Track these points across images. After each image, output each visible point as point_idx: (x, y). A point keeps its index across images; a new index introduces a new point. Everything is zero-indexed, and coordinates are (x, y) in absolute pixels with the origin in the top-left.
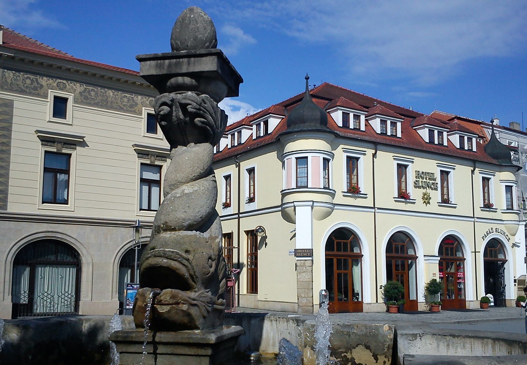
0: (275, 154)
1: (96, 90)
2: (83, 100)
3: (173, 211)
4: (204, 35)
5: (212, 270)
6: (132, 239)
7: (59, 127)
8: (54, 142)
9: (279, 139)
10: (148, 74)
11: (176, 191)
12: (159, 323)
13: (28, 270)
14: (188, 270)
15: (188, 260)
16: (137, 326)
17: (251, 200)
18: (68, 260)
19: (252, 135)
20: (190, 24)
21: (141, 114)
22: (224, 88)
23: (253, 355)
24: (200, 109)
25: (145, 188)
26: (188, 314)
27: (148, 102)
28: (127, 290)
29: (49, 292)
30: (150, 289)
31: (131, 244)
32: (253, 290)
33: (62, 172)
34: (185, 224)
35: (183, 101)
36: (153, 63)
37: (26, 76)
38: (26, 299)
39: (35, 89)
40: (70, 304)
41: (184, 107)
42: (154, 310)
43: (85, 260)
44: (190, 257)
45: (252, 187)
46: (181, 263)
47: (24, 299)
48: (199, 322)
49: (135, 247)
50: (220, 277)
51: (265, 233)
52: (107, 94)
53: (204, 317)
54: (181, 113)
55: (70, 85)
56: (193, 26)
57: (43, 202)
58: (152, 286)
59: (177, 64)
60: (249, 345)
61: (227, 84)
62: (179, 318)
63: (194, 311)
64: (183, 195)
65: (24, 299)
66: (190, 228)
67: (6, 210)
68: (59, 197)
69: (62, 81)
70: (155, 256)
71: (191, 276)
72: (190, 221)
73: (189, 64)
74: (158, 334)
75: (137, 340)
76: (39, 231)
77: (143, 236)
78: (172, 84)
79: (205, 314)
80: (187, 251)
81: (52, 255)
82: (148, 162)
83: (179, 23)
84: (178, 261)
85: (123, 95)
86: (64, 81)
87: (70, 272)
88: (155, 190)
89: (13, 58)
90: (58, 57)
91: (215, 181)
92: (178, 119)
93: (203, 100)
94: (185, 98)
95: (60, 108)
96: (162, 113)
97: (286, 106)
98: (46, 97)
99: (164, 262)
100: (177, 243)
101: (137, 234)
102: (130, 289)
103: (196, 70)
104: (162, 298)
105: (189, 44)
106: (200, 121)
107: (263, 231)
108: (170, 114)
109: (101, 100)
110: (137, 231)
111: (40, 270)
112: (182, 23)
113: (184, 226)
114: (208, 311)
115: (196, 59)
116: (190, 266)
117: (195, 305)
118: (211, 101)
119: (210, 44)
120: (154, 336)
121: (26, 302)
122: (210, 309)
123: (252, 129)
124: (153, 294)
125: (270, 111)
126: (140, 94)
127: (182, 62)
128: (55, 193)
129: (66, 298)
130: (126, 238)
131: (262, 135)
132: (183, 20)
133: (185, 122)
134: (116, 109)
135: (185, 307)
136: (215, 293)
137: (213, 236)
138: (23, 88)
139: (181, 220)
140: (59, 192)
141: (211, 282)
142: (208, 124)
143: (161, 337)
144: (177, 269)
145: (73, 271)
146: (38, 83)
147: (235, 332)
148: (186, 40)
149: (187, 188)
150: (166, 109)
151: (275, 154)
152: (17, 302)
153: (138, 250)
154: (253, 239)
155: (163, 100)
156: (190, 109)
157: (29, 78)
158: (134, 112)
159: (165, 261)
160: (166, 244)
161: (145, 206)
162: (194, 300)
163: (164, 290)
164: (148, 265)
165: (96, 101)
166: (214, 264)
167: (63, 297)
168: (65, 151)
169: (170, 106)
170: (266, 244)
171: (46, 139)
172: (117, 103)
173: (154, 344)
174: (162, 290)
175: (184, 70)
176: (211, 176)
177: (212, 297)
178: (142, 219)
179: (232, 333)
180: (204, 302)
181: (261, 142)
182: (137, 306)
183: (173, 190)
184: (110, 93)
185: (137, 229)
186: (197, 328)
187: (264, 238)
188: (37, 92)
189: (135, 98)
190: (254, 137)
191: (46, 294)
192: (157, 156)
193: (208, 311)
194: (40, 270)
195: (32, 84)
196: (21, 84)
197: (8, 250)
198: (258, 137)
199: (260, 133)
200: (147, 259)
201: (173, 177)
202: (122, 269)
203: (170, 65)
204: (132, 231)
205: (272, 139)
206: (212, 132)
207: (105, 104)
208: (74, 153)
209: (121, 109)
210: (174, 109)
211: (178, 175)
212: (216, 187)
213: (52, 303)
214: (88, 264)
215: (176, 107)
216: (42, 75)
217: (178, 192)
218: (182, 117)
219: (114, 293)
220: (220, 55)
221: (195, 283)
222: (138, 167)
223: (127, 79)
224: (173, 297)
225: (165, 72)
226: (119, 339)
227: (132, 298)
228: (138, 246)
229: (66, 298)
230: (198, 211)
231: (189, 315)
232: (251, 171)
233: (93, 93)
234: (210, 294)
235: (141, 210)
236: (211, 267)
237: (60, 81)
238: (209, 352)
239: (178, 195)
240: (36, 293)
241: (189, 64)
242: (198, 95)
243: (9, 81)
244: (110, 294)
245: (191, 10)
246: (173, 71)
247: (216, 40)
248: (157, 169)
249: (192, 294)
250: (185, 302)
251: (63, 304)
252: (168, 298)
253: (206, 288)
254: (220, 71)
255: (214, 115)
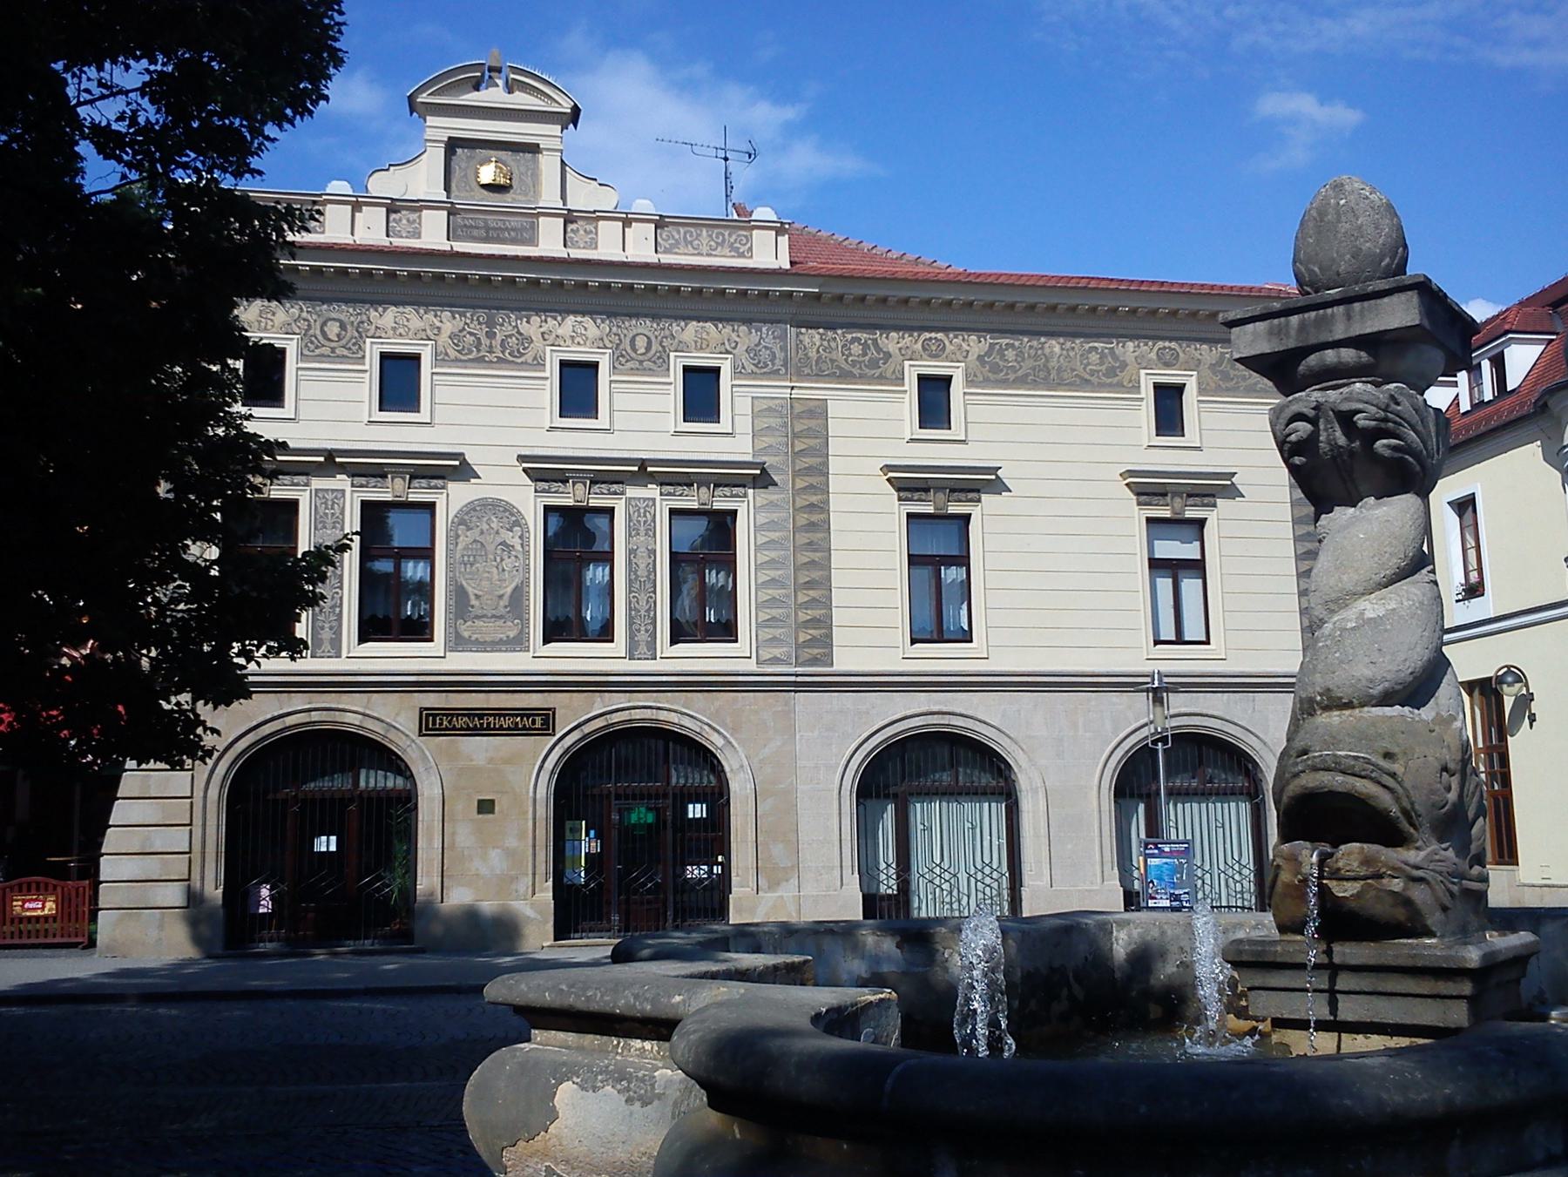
0: (1533, 451)
1: (1017, 344)
2: (991, 375)
3: (1342, 662)
4: (1374, 242)
5: (1452, 796)
6: (1146, 720)
7: (937, 453)
8: (927, 490)
9: (1545, 405)
10: (1253, 353)
11: (1343, 614)
12: (1340, 922)
13: (890, 808)
14: (1397, 799)
15: (1393, 775)
16: (1282, 929)
17: (1473, 590)
18: (984, 782)
19: (1456, 401)
20: (1339, 221)
21: (1136, 388)
22: (1438, 357)
23: (1554, 1014)
24: (1386, 420)
25: (1164, 585)
26: (1406, 902)
27: (1153, 355)
28: (1147, 856)
29: (946, 865)
30: (1308, 844)
31: (1145, 732)
32: (1501, 856)
33: (951, 561)
34: (1374, 692)
35: (1345, 407)
36: (1261, 326)
37: (849, 337)
38: (892, 882)
39: (874, 364)
40: (999, 894)
41: (1346, 419)
42: (1324, 892)
43: (1026, 780)
44: (1397, 767)
45: (1472, 554)
46: (1379, 783)
47: (888, 885)
48: (1434, 919)
49: (1155, 742)
50: (1471, 814)
51: (1527, 686)
52: (1047, 351)
53: (1445, 909)
54: (1339, 433)
55: (952, 342)
56: (1348, 226)
57: (913, 642)
58: (1312, 838)
59: (1318, 323)
60: (1541, 992)
61: (1441, 346)
62: (1383, 910)
63: (1418, 894)
64: (1364, 622)
65: (888, 885)
66: (1386, 699)
67: (832, 665)
68: (949, 625)
69: (933, 335)
70: (1315, 769)
71: (1405, 812)
72: (1387, 684)
73: (1349, 317)
74: (1337, 948)
75: (1288, 960)
76: (909, 713)
77: (1172, 712)
78: (1310, 369)
79: (1447, 901)
80: (1388, 755)
81: (944, 770)
82: (1165, 513)
83: (1311, 224)
84: (1371, 779)
85: (1087, 346)
86: (940, 335)
87: (992, 813)
88: (1190, 586)
89: (818, 297)
90: (920, 276)
91: (1436, 583)
92: (1334, 446)
93: (1392, 397)
94: (1347, 399)
95: (934, 401)
96: (1293, 438)
97: (1555, 305)
98: (900, 380)
99: (1338, 782)
100: (1362, 737)
101: (1158, 709)
102: (1153, 856)
103: (1368, 331)
104: (1340, 864)
105: (1342, 269)
106: (1388, 446)
107: (1520, 678)
108: (1313, 437)
109: (1034, 369)
110: (1158, 701)
111: (918, 810)
112: (1318, 223)
113: (1372, 697)
114: (1452, 894)
115: (1366, 304)
116: (1400, 790)
117: (1421, 880)
118: (1412, 396)
119: (1393, 258)
120: (1329, 952)
121: (893, 891)
122: (1455, 889)
123: (1455, 384)
124: (1320, 855)
125: (1507, 327)
126: (1132, 337)
127: (1333, 315)
128: (939, 611)
129: (988, 881)
130: (1129, 721)
131: (1488, 396)
132: (1322, 213)
133: (1352, 453)
134: (1071, 386)
135: (1397, 885)
136: (1463, 850)
137: (1445, 714)
138: (847, 367)
139: (1364, 682)
140: (948, 611)
141: (1452, 825)
142: (1408, 449)
143: (1344, 954)
144: (1370, 797)
145: (998, 809)
146: (879, 350)
147: (1522, 945)
148: (1333, 260)
149: (1371, 607)
150: (1303, 428)
151: (1533, 451)
152: (873, 891)
153: (1165, 750)
154: (1489, 705)
155: (1295, 408)
156: (1361, 421)
157: (854, 340)
158: (1119, 386)
159: (1340, 778)
160: (1334, 741)
161: (1168, 632)
162: (1417, 868)
163: (1342, 847)
164: (1298, 791)
165: (1020, 373)
166: (1455, 782)
167: (979, 876)
168: (954, 509)
169: (1313, 421)
170: (1532, 719)
171: (908, 485)
172: (1073, 370)
173: (1333, 969)
174: (1336, 845)
175: (1339, 333)
176: (1424, 571)
177: (1456, 860)
178: (1166, 667)
179: (1515, 947)
180: (1440, 873)
181: (1488, 418)
182: (1279, 883)
183: (1333, 612)
184: (1054, 346)
185: (1158, 695)
186: (1431, 934)
187: (1525, 701)
188: (876, 372)
189: (1119, 350)
190: (1465, 406)
191: (937, 870)
192: (1190, 496)
193: (1452, 894)
194: (918, 810)
195: (865, 354)
196: (841, 359)
197: (844, 762)
198: (1478, 405)
199: (1481, 392)
200: (1296, 775)
201: (1332, 582)
202: (869, 803)
203: (1303, 327)
204: (1142, 700)
205: (1522, 405)
206: (1418, 468)
207: (1044, 378)
208: (976, 512)
209: (1084, 383)
210: (1322, 427)
211: (1345, 578)
212: (1439, 596)
213: (955, 893)
214: (1035, 791)
215: (1328, 421)
216: (886, 328)
217: (1348, 617)
218: (1342, 440)
219: (1107, 867)
220: (1426, 290)
221: (1416, 829)
222: (1141, 529)
223: (1094, 303)
224: (1367, 861)
225: (1291, 344)
226: (1245, 958)
227: (1160, 879)
228: (1164, 740)
229: (988, 881)
230: (1400, 658)
231: (1407, 902)
232: (1465, 506)
233: (1010, 354)
234: (1451, 853)
235: (1157, 642)
236: (1449, 789)
237: (927, 335)
238: (1467, 988)
239: (1350, 625)
240: (914, 868)
241: (1349, 317)
242: (1377, 385)
243: (813, 354)
244: (1098, 868)
245: (1338, 187)
246: (1313, 341)
247: (1405, 247)
248: (1190, 531)
249: (1412, 855)
250: (1397, 872)
251: (980, 895)
252: (1356, 864)
253: (1441, 841)
254: (1426, 324)
255: (1420, 428)
